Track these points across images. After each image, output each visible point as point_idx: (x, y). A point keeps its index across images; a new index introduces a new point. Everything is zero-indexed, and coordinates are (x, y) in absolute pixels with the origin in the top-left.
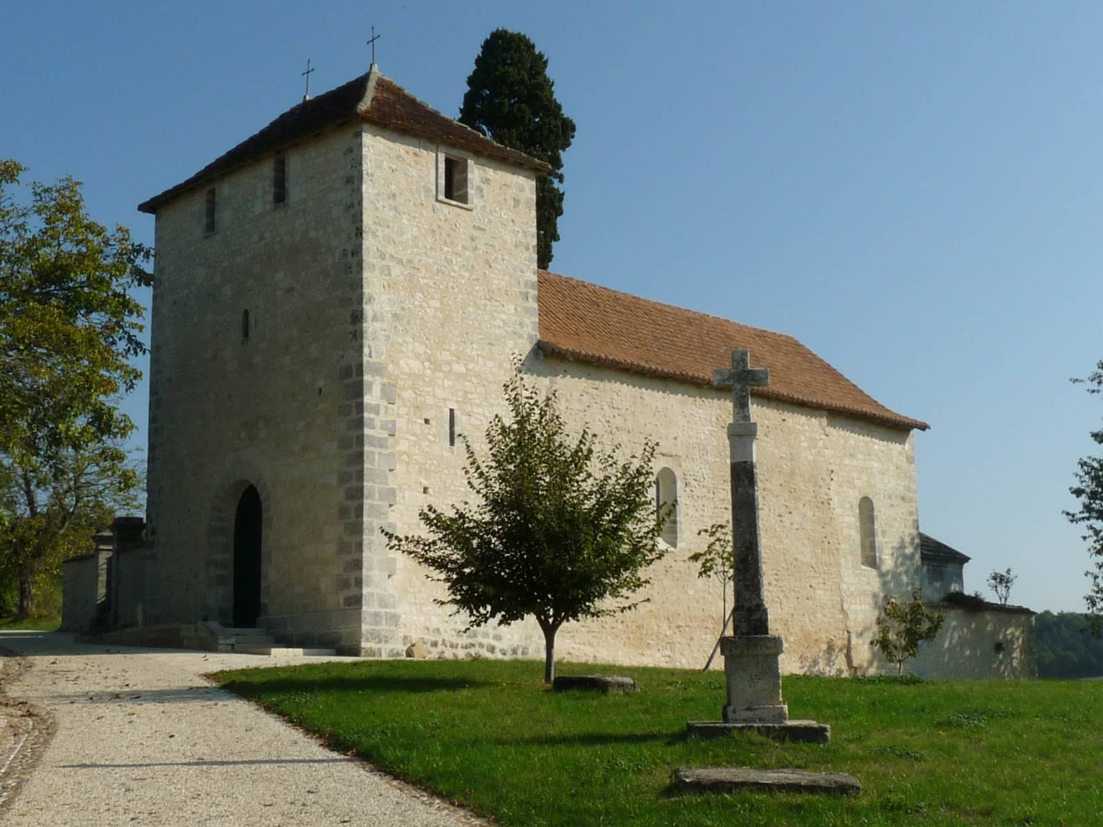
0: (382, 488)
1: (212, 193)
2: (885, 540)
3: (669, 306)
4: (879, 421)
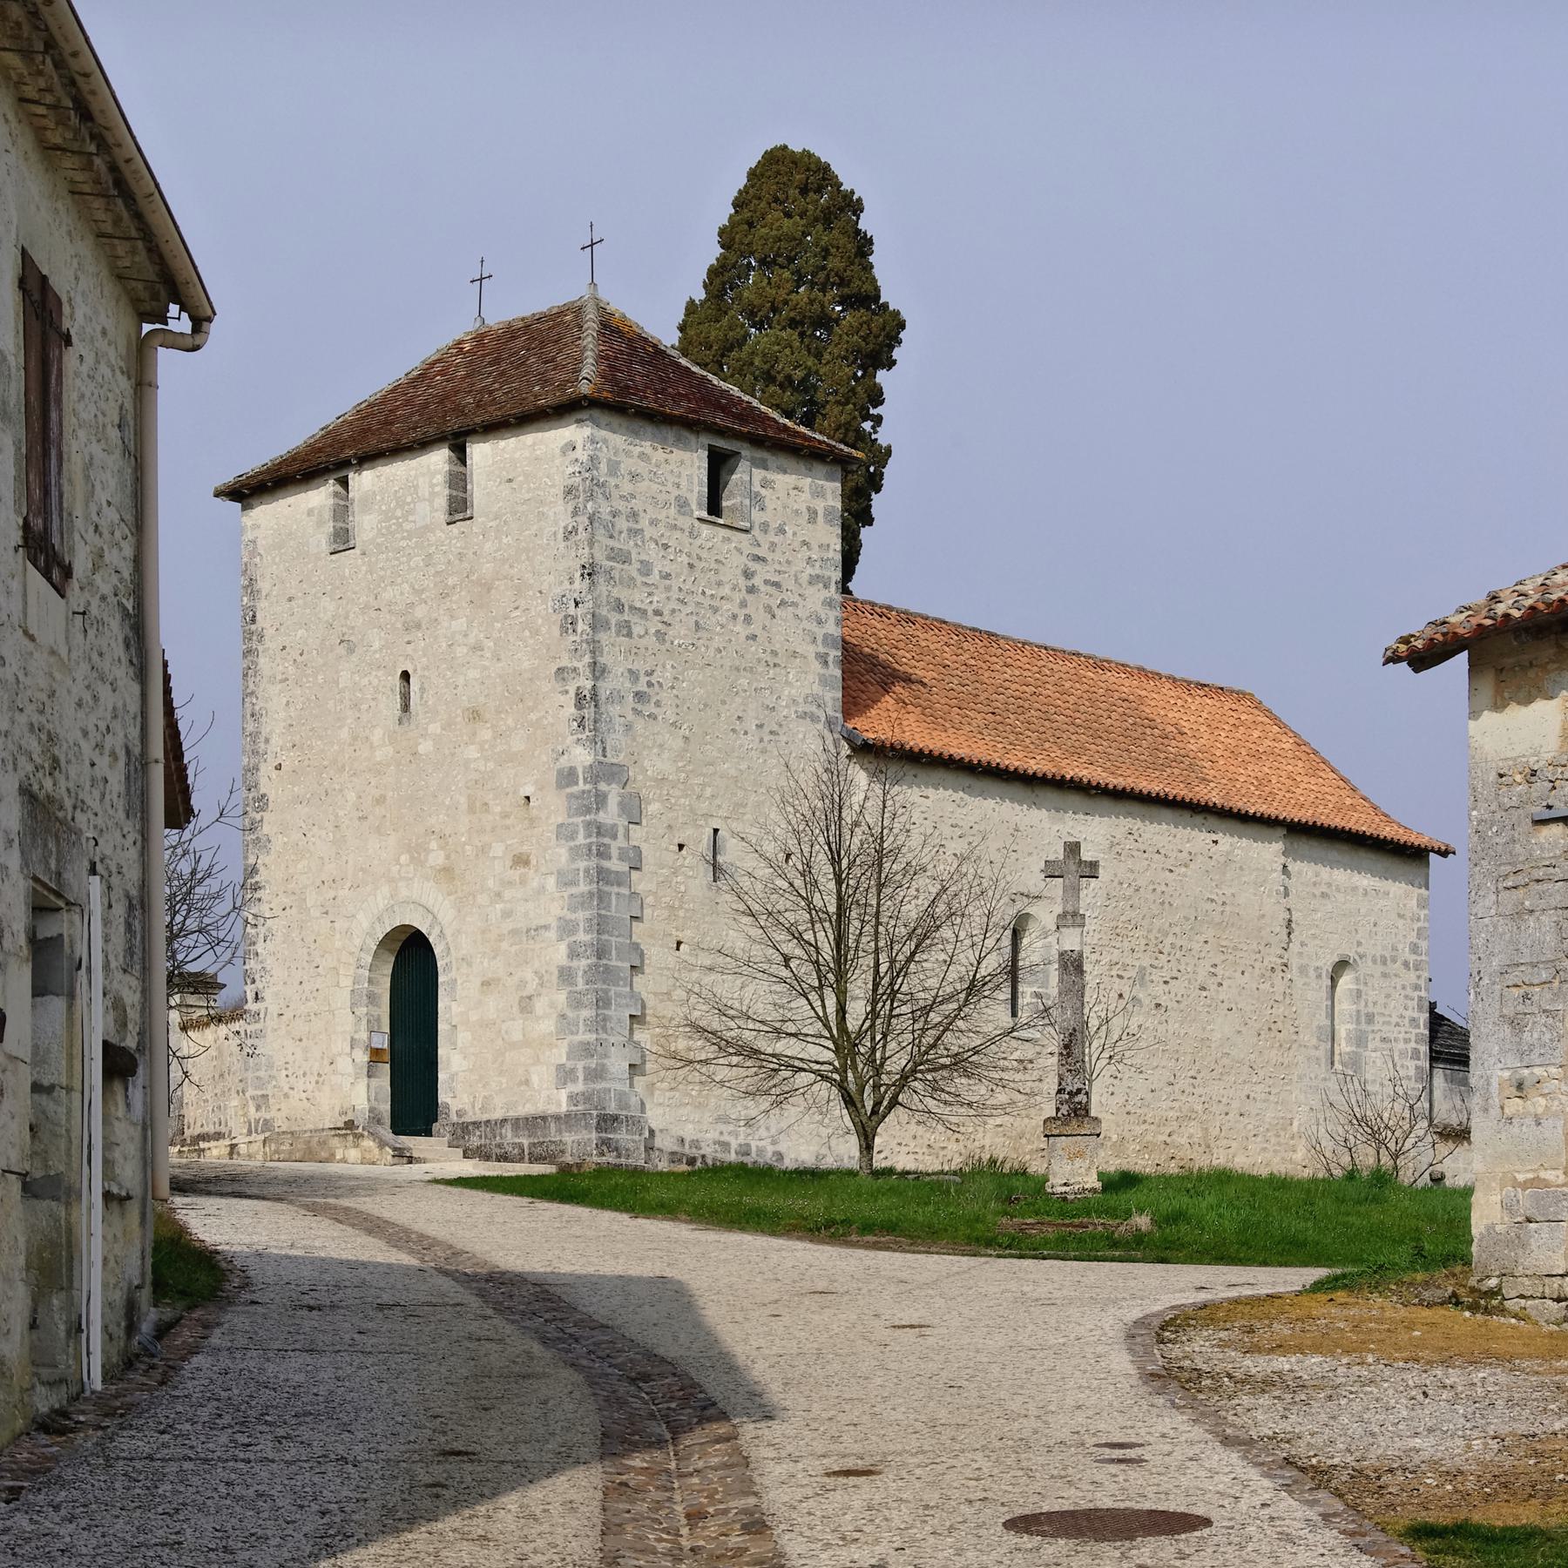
0: (622, 944)
1: (344, 483)
2: (1370, 1028)
3: (1044, 1258)
4: (1370, 842)
